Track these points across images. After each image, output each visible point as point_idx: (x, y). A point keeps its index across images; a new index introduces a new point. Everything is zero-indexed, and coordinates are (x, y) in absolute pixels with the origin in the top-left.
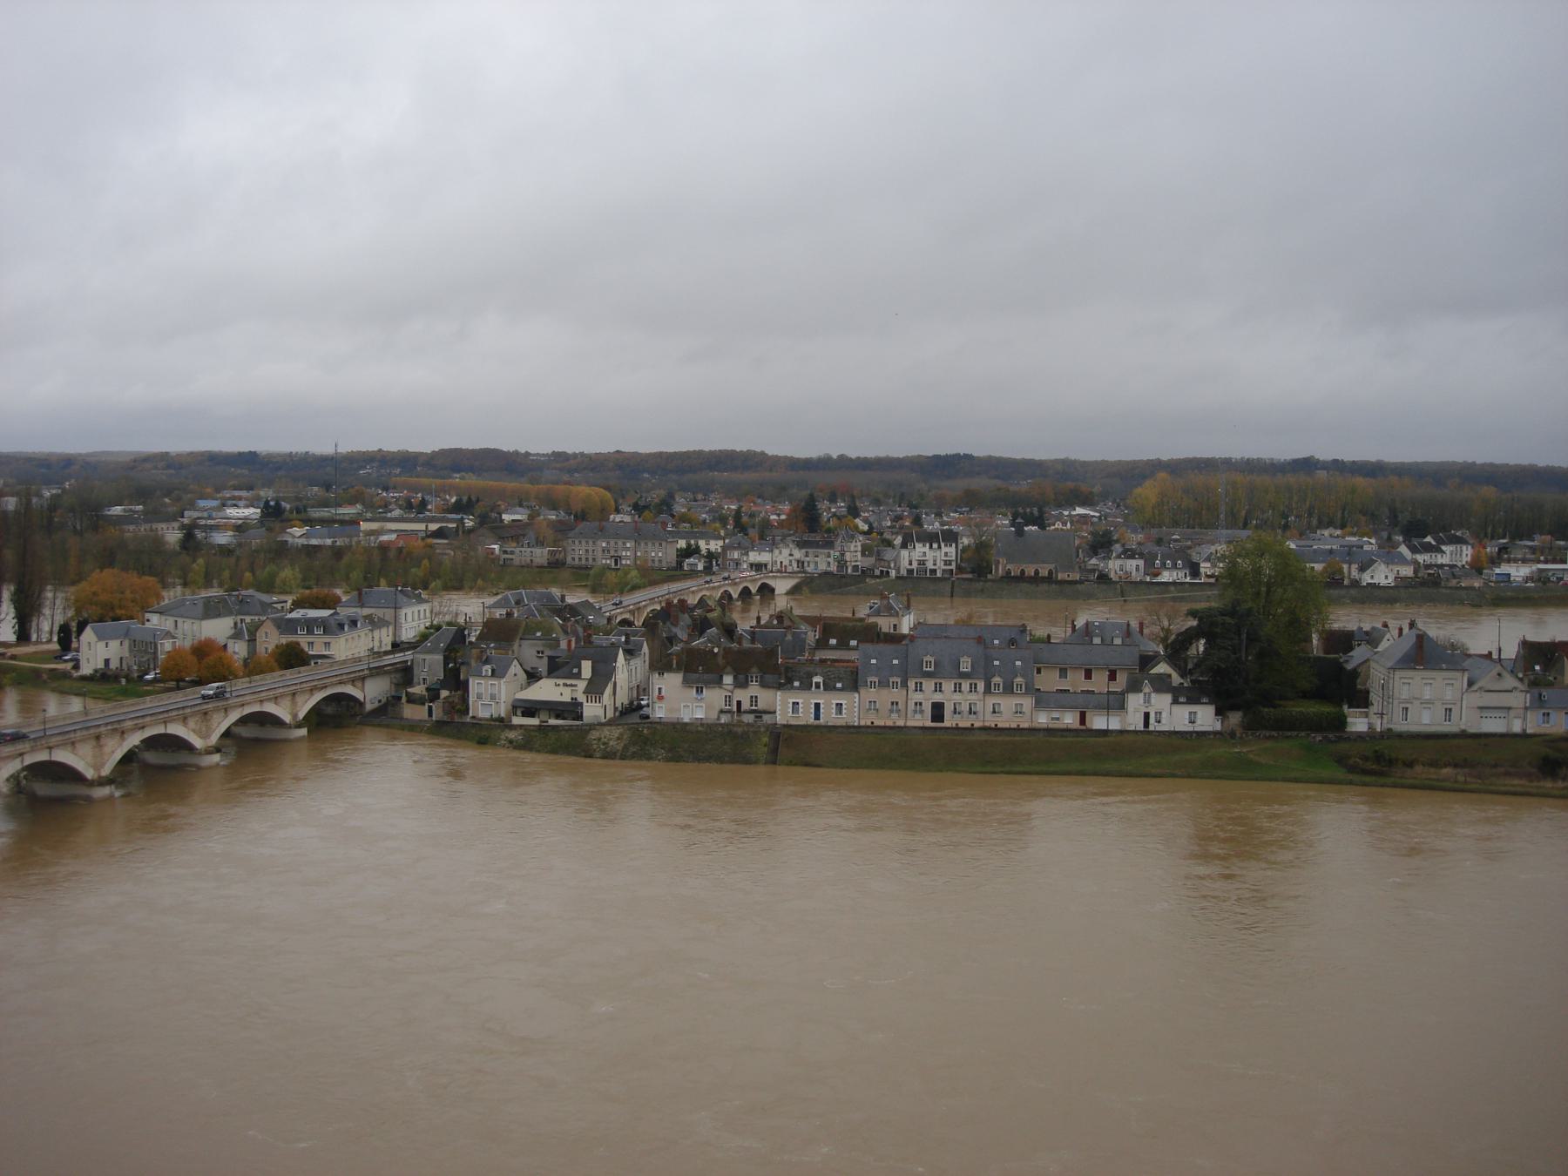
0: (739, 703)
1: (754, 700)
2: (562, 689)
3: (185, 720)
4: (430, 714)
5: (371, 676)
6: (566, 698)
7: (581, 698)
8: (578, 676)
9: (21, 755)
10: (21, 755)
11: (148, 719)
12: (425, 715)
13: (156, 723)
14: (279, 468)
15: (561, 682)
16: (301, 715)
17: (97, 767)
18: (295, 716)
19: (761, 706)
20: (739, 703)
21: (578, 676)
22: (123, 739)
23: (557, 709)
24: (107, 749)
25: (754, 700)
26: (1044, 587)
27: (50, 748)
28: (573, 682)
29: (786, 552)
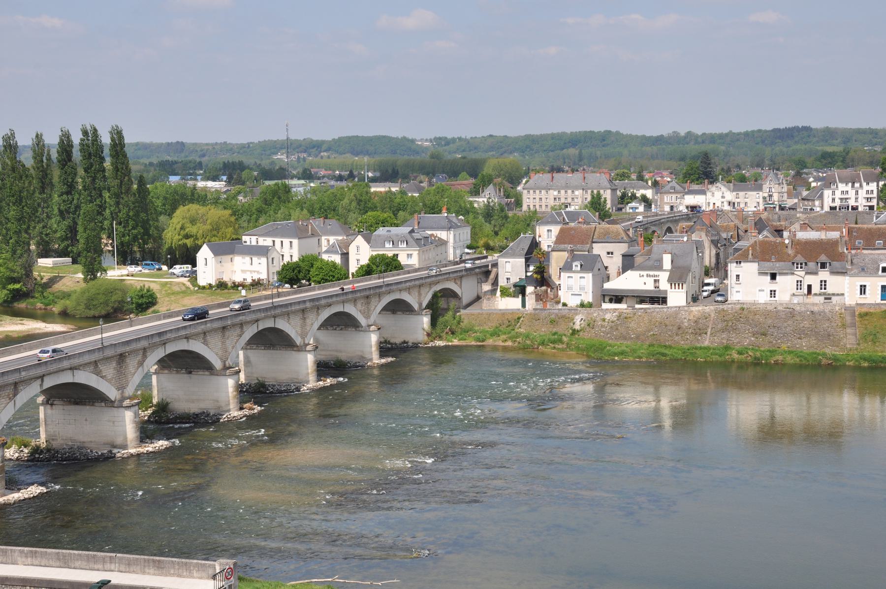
0: (809, 287)
1: (823, 284)
2: (645, 279)
3: (355, 301)
4: (524, 305)
5: (467, 275)
6: (650, 286)
7: (664, 285)
8: (660, 268)
9: (257, 321)
10: (257, 321)
11: (334, 299)
12: (519, 306)
13: (338, 303)
14: (117, 167)
15: (645, 273)
16: (424, 305)
17: (121, 388)
18: (420, 305)
19: (830, 290)
20: (809, 287)
21: (660, 268)
22: (318, 314)
23: (643, 298)
24: (308, 321)
25: (823, 284)
26: (750, 372)
27: (275, 317)
28: (656, 273)
29: (718, 194)
